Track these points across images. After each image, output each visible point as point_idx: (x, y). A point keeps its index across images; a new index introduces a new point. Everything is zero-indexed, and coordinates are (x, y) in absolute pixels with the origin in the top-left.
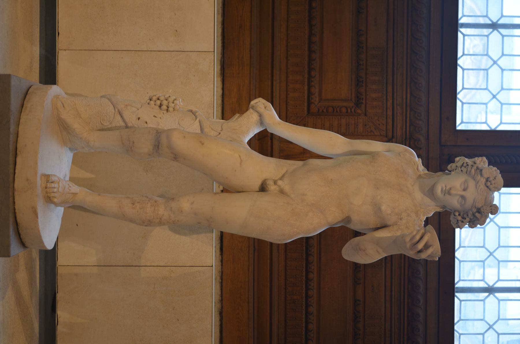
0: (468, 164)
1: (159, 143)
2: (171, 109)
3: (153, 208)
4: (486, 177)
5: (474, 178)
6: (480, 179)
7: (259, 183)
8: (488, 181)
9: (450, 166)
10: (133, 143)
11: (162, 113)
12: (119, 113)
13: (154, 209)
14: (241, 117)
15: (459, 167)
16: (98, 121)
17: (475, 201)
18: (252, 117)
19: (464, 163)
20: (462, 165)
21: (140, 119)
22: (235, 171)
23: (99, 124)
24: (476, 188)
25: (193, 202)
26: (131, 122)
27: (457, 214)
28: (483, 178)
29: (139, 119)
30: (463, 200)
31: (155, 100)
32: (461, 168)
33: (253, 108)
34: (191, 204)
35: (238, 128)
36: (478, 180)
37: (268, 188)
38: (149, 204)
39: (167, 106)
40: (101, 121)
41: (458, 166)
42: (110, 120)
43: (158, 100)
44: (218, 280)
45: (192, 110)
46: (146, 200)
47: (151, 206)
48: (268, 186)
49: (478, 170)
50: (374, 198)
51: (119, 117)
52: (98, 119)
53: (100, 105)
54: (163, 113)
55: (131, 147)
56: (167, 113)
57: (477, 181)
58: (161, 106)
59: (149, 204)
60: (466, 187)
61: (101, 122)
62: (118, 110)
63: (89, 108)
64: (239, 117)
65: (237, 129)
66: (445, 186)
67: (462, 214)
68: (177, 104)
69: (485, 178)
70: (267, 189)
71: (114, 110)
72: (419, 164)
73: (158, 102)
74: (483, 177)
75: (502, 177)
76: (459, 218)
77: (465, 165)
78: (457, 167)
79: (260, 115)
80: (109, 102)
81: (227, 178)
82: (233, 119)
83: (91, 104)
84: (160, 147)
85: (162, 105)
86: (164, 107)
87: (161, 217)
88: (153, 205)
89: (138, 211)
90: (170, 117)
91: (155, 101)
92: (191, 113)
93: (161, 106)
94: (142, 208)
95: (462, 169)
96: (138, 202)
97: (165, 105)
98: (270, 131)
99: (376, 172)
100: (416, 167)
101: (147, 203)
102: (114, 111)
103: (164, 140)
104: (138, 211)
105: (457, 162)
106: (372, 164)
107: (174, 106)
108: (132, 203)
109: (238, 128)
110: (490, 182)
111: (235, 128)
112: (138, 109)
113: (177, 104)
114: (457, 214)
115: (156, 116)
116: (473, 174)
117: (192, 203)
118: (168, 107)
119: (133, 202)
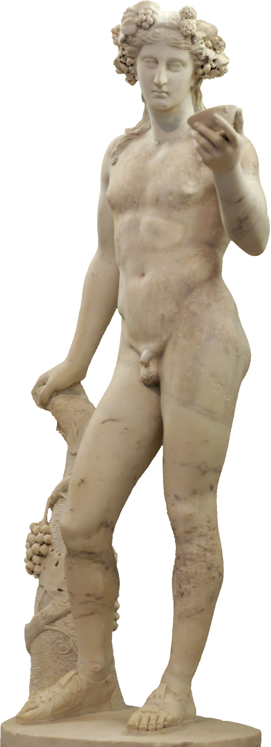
0: (122, 56)
1: (84, 552)
2: (46, 537)
3: (188, 562)
5: (139, 48)
6: (139, 38)
7: (146, 390)
8: (141, 26)
9: (130, 83)
10: (88, 595)
11: (53, 552)
14: (60, 424)
15: (129, 69)
16: (66, 658)
17: (173, 45)
18: (59, 405)
19: (121, 62)
20: (125, 64)
21: (61, 588)
22: (126, 429)
23: (70, 657)
24: (152, 43)
25: (175, 496)
28: (138, 32)
29: (60, 590)
31: (32, 564)
32: (129, 66)
33: (46, 405)
34: (179, 500)
35: (76, 429)
36: (141, 41)
37: (153, 376)
38: (182, 568)
39: (41, 545)
40: (66, 652)
41: (127, 71)
42: (64, 638)
43: (33, 559)
46: (177, 574)
47: (184, 565)
48: (149, 377)
51: (59, 626)
52: (63, 657)
53: (40, 654)
54: (52, 550)
55: (97, 599)
56: (53, 544)
57: (143, 42)
58: (40, 555)
59: (182, 568)
60: (153, 60)
61: (67, 654)
62: (47, 624)
64: (60, 428)
65: (78, 430)
66: (153, 92)
67: (200, 63)
68: (39, 529)
69: (137, 30)
70: (154, 378)
71: (46, 632)
75: (136, 3)
76: (208, 66)
77: (121, 59)
78: (128, 72)
80: (35, 640)
84: (89, 550)
85: (40, 552)
87: (203, 549)
89: (194, 587)
90: (58, 539)
91: (35, 564)
93: (40, 555)
94: (189, 580)
95: (129, 65)
97: (40, 547)
98: (84, 376)
99: (135, 203)
100: (134, 136)
101: (181, 571)
102: (49, 632)
103: (79, 544)
104: (194, 587)
105: (122, 71)
106: (123, 210)
107: (41, 533)
108: (182, 596)
109: (76, 427)
110: (142, 23)
111: (76, 432)
113: (39, 529)
114: (200, 71)
115: (55, 562)
116: (134, 48)
117: (177, 497)
118: (44, 543)
119: (180, 595)
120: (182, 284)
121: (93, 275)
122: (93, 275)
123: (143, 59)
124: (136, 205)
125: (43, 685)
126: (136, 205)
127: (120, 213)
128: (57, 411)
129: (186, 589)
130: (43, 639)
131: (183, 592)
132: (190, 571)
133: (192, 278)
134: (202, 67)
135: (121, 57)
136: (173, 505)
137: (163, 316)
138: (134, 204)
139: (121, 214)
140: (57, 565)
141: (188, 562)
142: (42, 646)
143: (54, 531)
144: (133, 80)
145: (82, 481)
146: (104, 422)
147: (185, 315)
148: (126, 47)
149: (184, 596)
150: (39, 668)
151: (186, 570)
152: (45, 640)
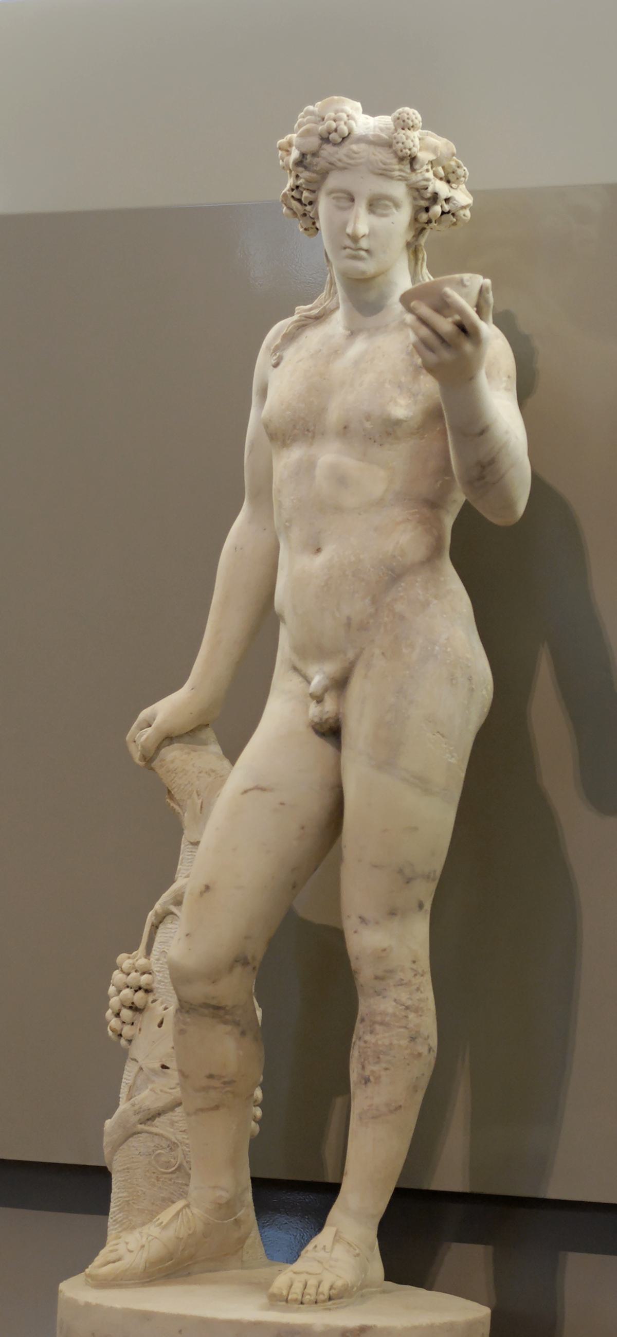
1: (206, 1005)
3: (378, 1027)
4: (320, 142)
5: (324, 175)
6: (324, 158)
8: (328, 138)
10: (211, 1076)
12: (148, 1120)
13: (382, 1023)
14: (173, 792)
15: (305, 210)
16: (170, 1180)
17: (380, 172)
18: (173, 762)
20: (299, 200)
22: (282, 804)
23: (177, 1178)
24: (345, 168)
25: (360, 917)
26: (171, 1089)
27: (139, 998)
29: (164, 1067)
30: (382, 202)
31: (120, 1023)
32: (305, 205)
34: (366, 924)
35: (200, 801)
38: (368, 1037)
39: (136, 991)
40: (170, 1170)
42: (168, 1146)
44: (186, 815)
45: (153, 925)
47: (371, 1032)
48: (323, 720)
49: (304, 163)
50: (370, 439)
51: (161, 1126)
52: (165, 1178)
53: (128, 1172)
54: (154, 1001)
55: (225, 1083)
56: (155, 990)
57: (330, 166)
58: (133, 1008)
59: (368, 1037)
60: (346, 196)
61: (172, 1173)
62: (141, 1122)
63: (133, 1201)
65: (202, 803)
66: (345, 248)
67: (424, 203)
69: (320, 146)
70: (331, 721)
71: (139, 1135)
72: (305, 314)
73: (126, 1014)
74: (318, 152)
79: (169, 739)
80: (121, 1148)
81: (303, 828)
82: (179, 813)
83: (125, 1197)
84: (214, 1002)
85: (133, 1003)
86: (139, 998)
87: (404, 1007)
88: (371, 1026)
89: (386, 1069)
91: (124, 1022)
92: (161, 926)
93: (133, 1008)
94: (379, 1058)
95: (307, 203)
96: (363, 1068)
97: (134, 995)
99: (308, 430)
100: (311, 321)
101: (365, 1042)
102: (144, 1135)
103: (198, 991)
104: (386, 1069)
106: (288, 442)
107: (136, 971)
108: (366, 1083)
109: (199, 799)
110: (330, 133)
112: (141, 1069)
114: (424, 217)
115: (158, 1021)
116: (314, 175)
117: (363, 920)
118: (140, 988)
119: (363, 1082)
120: (382, 567)
121: (236, 548)
122: (236, 548)
123: (331, 192)
124: (310, 435)
125: (131, 1223)
126: (310, 435)
127: (283, 447)
128: (168, 772)
129: (373, 1072)
130: (133, 1146)
131: (367, 1077)
132: (380, 1042)
133: (399, 558)
134: (427, 210)
135: (293, 190)
136: (355, 932)
137: (349, 619)
138: (306, 433)
139: (284, 448)
140: (160, 1025)
141: (378, 1028)
142: (133, 1158)
143: (158, 969)
144: (312, 228)
145: (207, 888)
146: (246, 792)
147: (386, 619)
148: (302, 172)
149: (369, 1084)
150: (125, 1194)
151: (373, 1041)
152: (137, 1150)
